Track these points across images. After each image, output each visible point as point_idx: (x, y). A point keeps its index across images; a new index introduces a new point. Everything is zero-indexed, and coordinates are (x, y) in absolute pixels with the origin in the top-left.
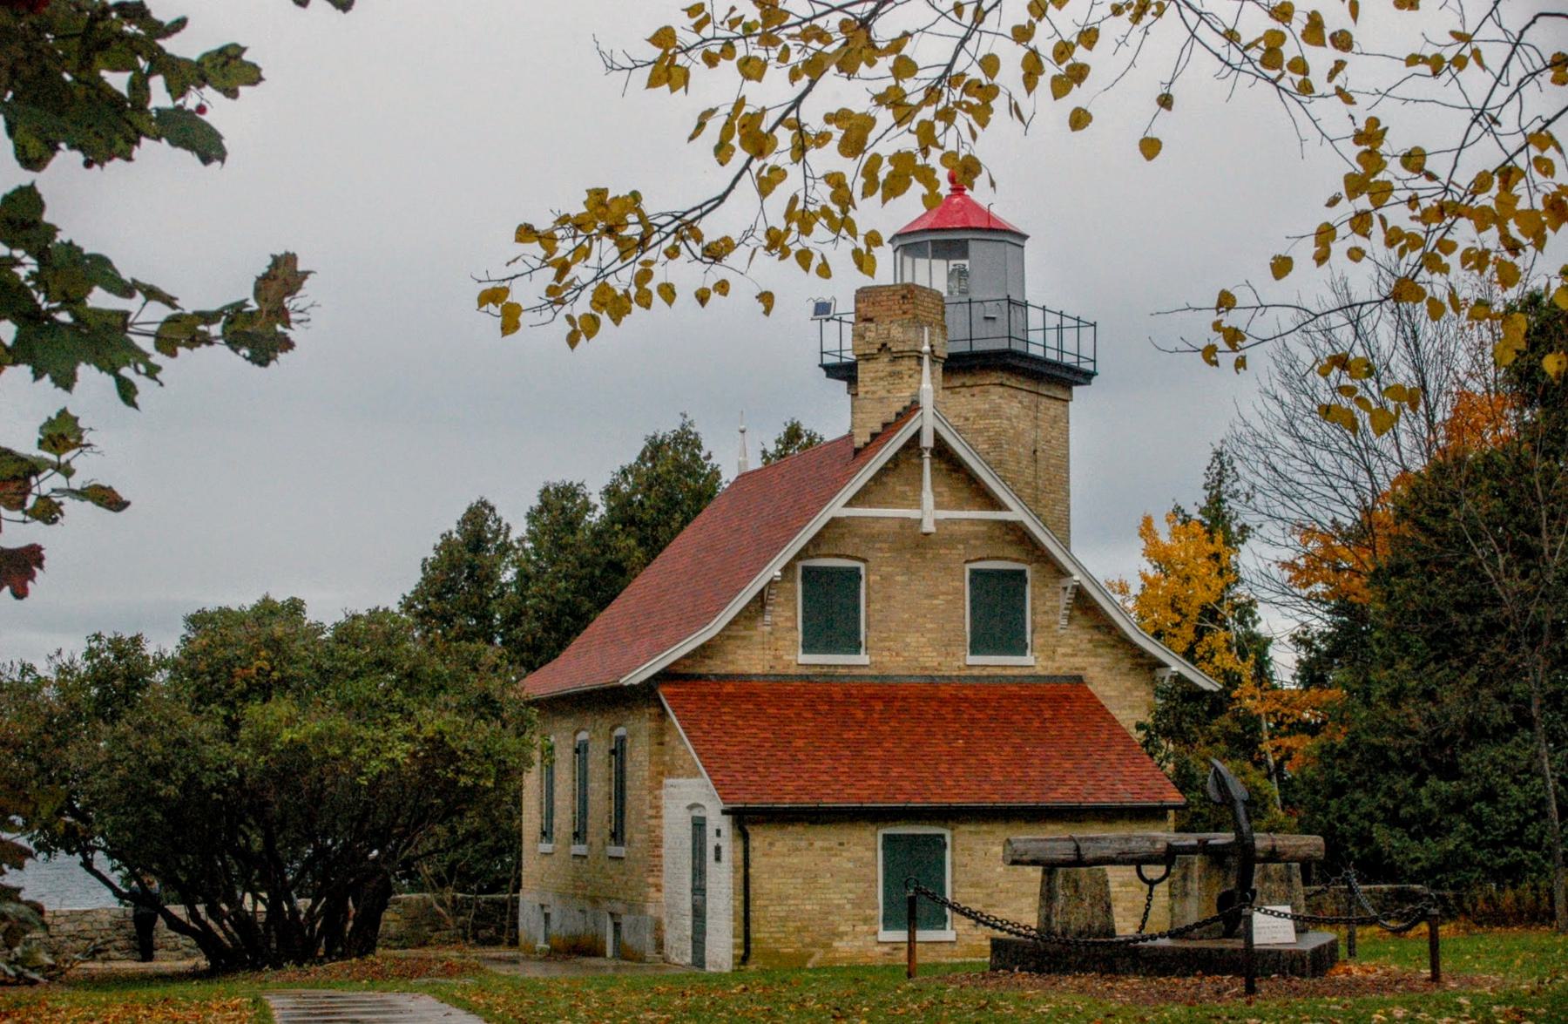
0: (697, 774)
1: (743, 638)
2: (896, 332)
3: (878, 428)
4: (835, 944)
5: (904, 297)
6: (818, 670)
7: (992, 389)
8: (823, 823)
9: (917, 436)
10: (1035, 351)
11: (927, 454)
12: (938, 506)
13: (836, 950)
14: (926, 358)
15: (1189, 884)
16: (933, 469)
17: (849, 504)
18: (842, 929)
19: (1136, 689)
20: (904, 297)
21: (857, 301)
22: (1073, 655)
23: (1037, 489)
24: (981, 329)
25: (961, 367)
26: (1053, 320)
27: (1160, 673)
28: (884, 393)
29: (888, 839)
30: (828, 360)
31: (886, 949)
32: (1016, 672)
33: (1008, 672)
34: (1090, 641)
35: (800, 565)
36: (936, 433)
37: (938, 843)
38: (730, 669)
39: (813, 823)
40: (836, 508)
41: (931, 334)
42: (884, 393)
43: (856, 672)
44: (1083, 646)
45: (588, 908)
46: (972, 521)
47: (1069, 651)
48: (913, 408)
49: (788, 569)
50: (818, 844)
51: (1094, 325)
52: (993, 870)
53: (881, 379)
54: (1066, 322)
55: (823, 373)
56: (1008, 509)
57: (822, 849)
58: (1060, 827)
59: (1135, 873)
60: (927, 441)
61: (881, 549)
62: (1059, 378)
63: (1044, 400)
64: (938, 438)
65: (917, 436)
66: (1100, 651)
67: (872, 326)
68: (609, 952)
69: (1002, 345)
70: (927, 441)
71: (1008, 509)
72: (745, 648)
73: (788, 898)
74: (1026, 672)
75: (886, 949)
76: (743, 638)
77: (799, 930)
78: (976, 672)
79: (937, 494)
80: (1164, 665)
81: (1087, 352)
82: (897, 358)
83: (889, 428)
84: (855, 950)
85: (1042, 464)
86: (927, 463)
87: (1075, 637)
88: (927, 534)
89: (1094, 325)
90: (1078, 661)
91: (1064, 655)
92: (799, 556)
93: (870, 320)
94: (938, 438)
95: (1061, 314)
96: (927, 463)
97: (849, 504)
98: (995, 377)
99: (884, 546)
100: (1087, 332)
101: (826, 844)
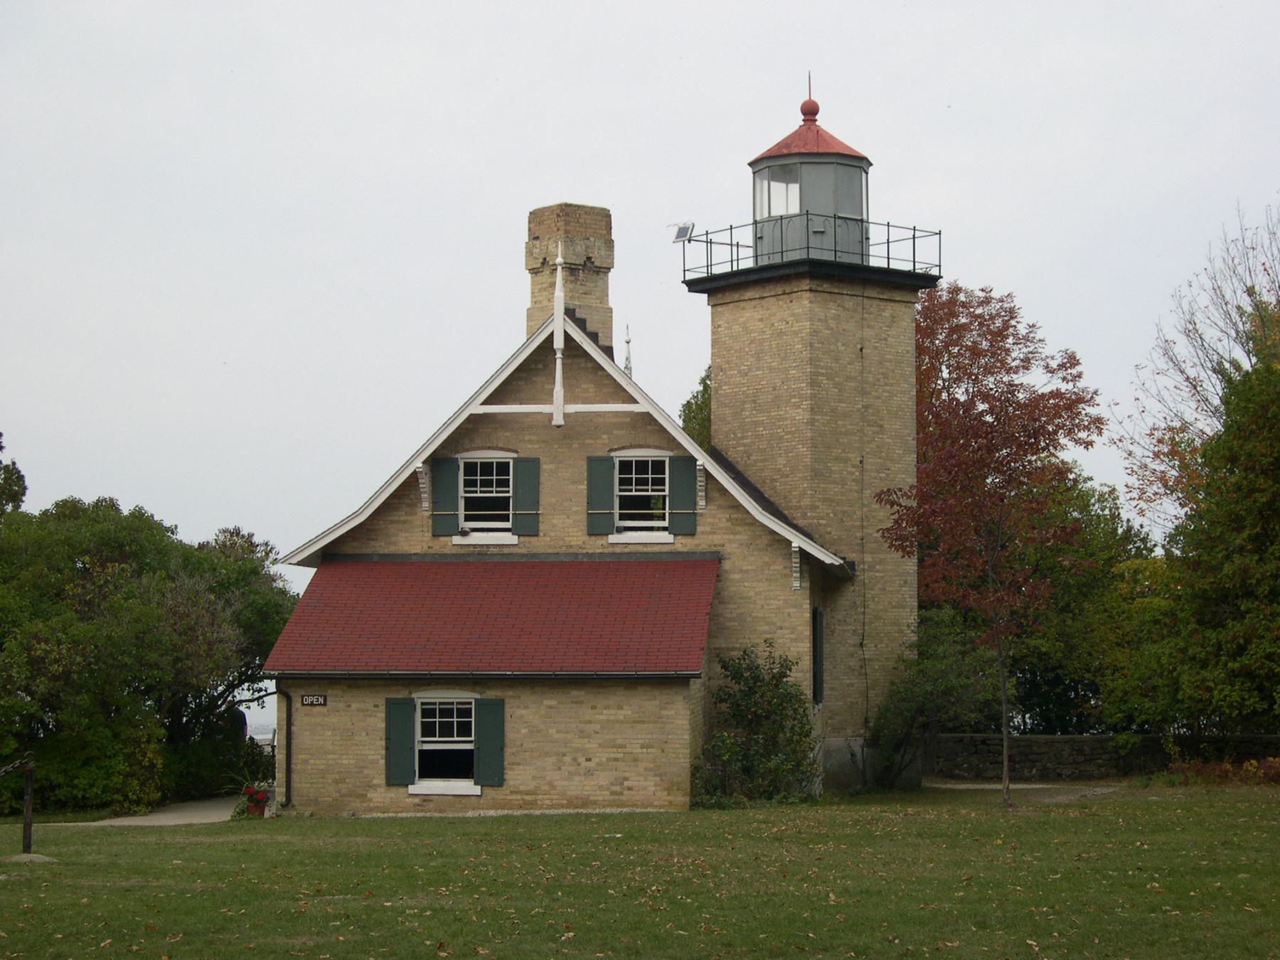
1: (405, 522)
8: (358, 687)
11: (559, 355)
12: (568, 400)
13: (371, 800)
17: (485, 403)
18: (375, 782)
19: (774, 563)
29: (387, 699)
30: (690, 276)
31: (417, 800)
32: (656, 549)
34: (728, 520)
35: (465, 457)
37: (500, 704)
38: (392, 549)
39: (350, 687)
43: (506, 551)
44: (721, 525)
45: (588, 764)
46: (616, 414)
47: (708, 529)
50: (354, 706)
55: (685, 288)
57: (358, 710)
58: (583, 693)
60: (559, 343)
61: (530, 441)
64: (568, 338)
66: (739, 528)
70: (559, 343)
71: (635, 402)
74: (665, 549)
75: (417, 800)
76: (405, 522)
77: (336, 782)
78: (618, 550)
86: (559, 362)
87: (714, 516)
88: (559, 427)
90: (717, 539)
91: (702, 533)
96: (559, 362)
98: (806, 284)
99: (533, 438)
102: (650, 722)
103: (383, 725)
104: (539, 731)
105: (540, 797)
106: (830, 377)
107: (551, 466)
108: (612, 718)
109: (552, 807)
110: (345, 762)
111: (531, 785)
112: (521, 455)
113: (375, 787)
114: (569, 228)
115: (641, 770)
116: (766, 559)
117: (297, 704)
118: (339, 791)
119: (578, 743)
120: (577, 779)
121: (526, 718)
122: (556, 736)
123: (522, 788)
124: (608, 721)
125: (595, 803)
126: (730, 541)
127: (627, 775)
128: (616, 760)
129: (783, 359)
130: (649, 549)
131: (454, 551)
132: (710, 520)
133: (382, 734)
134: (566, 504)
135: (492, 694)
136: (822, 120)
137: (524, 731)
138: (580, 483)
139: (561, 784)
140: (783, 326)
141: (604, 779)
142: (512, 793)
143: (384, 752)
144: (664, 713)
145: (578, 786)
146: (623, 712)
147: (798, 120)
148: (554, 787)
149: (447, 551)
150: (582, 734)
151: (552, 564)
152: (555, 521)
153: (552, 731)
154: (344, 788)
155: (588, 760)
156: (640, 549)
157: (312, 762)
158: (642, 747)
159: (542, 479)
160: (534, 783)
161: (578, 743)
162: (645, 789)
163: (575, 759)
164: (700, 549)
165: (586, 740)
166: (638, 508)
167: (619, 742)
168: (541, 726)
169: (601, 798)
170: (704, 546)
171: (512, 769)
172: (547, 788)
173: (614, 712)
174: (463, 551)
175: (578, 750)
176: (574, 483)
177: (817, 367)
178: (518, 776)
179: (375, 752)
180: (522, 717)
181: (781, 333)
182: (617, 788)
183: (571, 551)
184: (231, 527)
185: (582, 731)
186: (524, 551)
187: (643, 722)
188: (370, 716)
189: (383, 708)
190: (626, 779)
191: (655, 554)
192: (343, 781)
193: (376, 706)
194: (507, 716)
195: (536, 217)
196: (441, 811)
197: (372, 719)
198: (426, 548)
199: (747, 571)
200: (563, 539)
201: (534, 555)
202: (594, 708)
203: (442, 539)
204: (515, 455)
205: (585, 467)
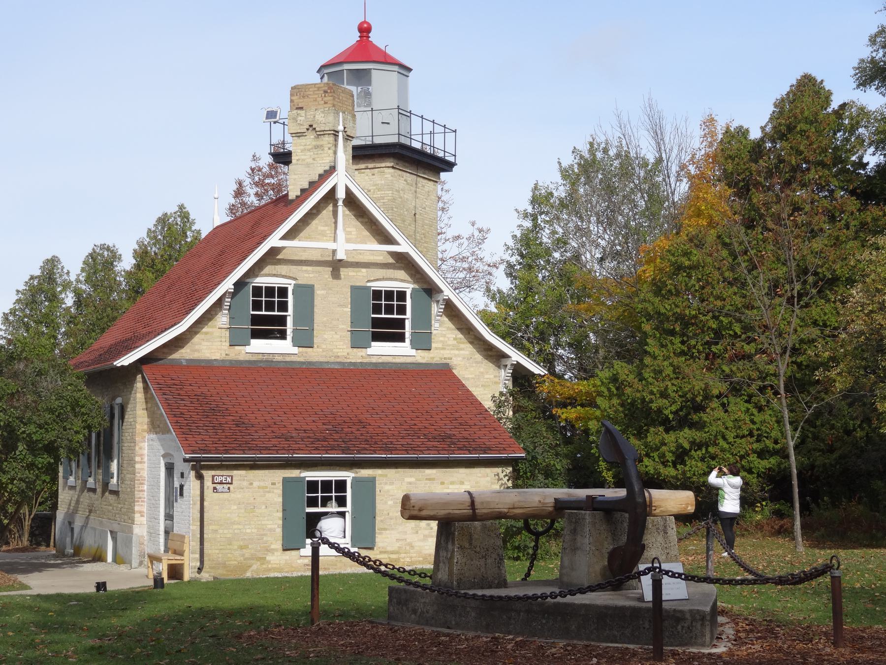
0: (169, 431)
2: (320, 117)
3: (306, 185)
4: (268, 558)
5: (325, 92)
6: (261, 357)
7: (387, 170)
9: (333, 191)
10: (416, 145)
11: (340, 203)
12: (348, 241)
13: (269, 562)
14: (341, 134)
15: (579, 538)
16: (344, 215)
18: (273, 547)
20: (325, 92)
21: (292, 95)
22: (444, 349)
24: (379, 129)
25: (364, 154)
26: (428, 127)
27: (505, 361)
28: (310, 161)
38: (196, 356)
40: (274, 240)
41: (344, 120)
42: (310, 161)
43: (288, 359)
44: (450, 343)
47: (440, 345)
48: (333, 169)
49: (240, 285)
50: (256, 484)
51: (455, 131)
52: (386, 503)
53: (309, 150)
54: (438, 129)
56: (398, 244)
57: (259, 487)
60: (341, 194)
62: (431, 165)
63: (421, 180)
64: (348, 192)
65: (333, 191)
66: (462, 346)
67: (302, 112)
68: (110, 558)
69: (394, 139)
70: (341, 194)
71: (398, 244)
72: (208, 340)
73: (233, 523)
79: (348, 233)
80: (508, 357)
81: (450, 149)
82: (320, 134)
83: (314, 186)
84: (283, 562)
85: (419, 222)
88: (340, 261)
89: (455, 131)
90: (446, 353)
91: (436, 348)
92: (253, 272)
93: (301, 108)
94: (348, 192)
95: (433, 122)
97: (284, 238)
100: (450, 136)
101: (262, 484)
103: (281, 499)
107: (323, 292)
110: (248, 531)
111: (395, 546)
112: (300, 282)
113: (272, 551)
116: (482, 370)
117: (208, 483)
118: (243, 555)
123: (389, 549)
126: (456, 356)
130: (398, 360)
131: (247, 359)
132: (442, 339)
133: (280, 508)
134: (334, 322)
135: (365, 473)
136: (374, 37)
137: (390, 503)
138: (344, 306)
142: (381, 552)
143: (281, 522)
147: (355, 36)
148: (412, 547)
149: (241, 358)
151: (302, 370)
152: (326, 336)
154: (247, 553)
156: (390, 360)
157: (221, 531)
159: (316, 302)
160: (398, 545)
164: (434, 361)
166: (388, 330)
171: (380, 534)
173: (457, 486)
174: (254, 358)
176: (340, 306)
179: (274, 522)
180: (388, 491)
183: (338, 360)
186: (301, 359)
188: (269, 492)
189: (280, 486)
191: (401, 364)
192: (246, 547)
193: (273, 484)
194: (378, 492)
195: (292, 88)
200: (331, 350)
201: (310, 363)
202: (442, 483)
203: (237, 347)
204: (293, 282)
205: (349, 294)
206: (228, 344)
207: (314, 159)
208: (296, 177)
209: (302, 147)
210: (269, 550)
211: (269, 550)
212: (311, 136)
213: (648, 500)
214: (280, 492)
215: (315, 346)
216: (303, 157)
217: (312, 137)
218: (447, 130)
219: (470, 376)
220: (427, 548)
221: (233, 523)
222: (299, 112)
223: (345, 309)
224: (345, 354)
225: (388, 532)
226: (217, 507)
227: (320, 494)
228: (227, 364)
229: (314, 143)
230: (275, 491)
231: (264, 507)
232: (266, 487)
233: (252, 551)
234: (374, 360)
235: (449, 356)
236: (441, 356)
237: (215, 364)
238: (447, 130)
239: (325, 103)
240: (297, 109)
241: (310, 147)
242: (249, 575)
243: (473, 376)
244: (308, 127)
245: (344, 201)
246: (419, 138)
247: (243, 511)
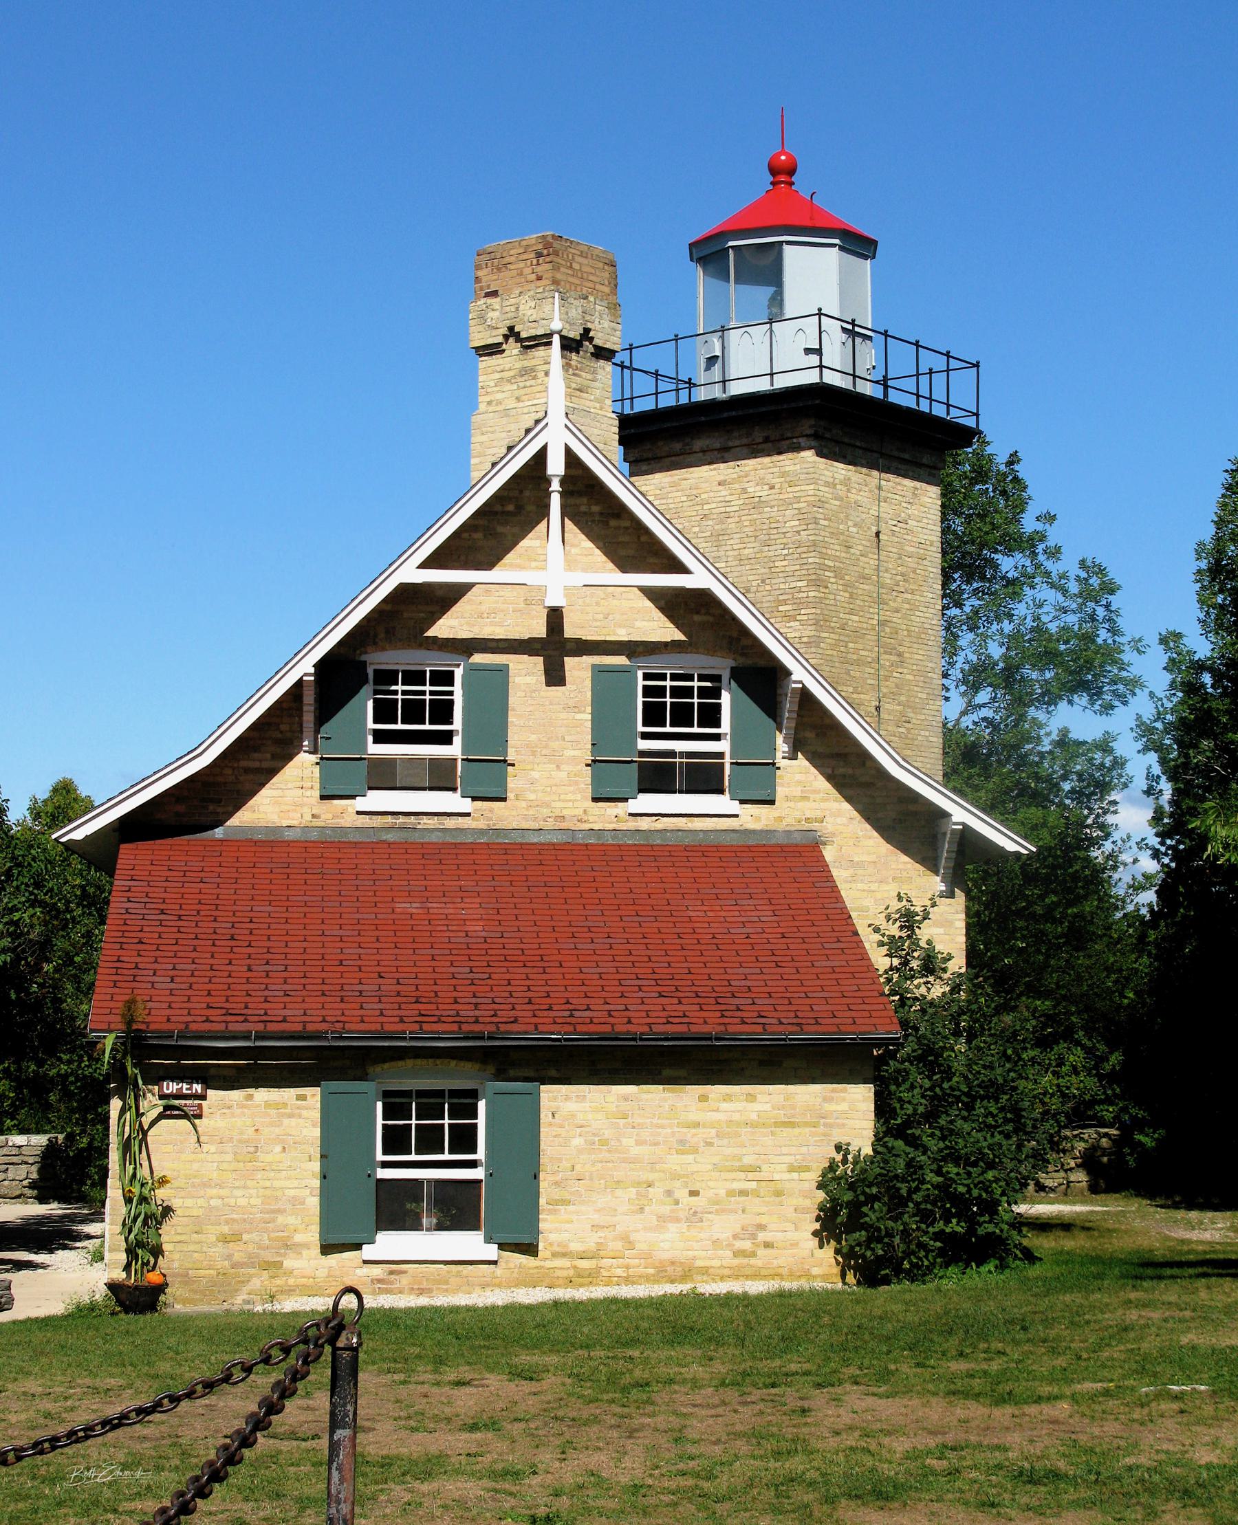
4: (288, 1264)
5: (539, 255)
11: (555, 485)
17: (424, 565)
18: (298, 1238)
23: (879, 585)
28: (511, 403)
33: (698, 824)
36: (569, 452)
42: (511, 403)
47: (797, 791)
51: (977, 365)
53: (509, 381)
59: (365, 1301)
60: (556, 466)
64: (571, 459)
70: (556, 466)
71: (686, 571)
73: (206, 1185)
75: (377, 1271)
77: (225, 1239)
89: (977, 365)
90: (810, 809)
91: (788, 798)
93: (494, 294)
94: (571, 459)
95: (917, 344)
102: (806, 1124)
103: (317, 1132)
104: (604, 1142)
105: (606, 1262)
106: (839, 574)
108: (736, 1117)
109: (629, 1280)
110: (242, 1202)
111: (590, 1243)
114: (559, 276)
115: (790, 1213)
118: (229, 1257)
119: (675, 1162)
120: (673, 1227)
121: (574, 1114)
122: (636, 1151)
123: (575, 1247)
124: (730, 1122)
125: (705, 1271)
127: (764, 1220)
128: (743, 1193)
129: (766, 544)
132: (798, 777)
134: (555, 745)
136: (803, 184)
137: (577, 1142)
138: (577, 709)
139: (643, 1240)
140: (764, 492)
141: (724, 1227)
143: (317, 1183)
144: (829, 1107)
145: (671, 1243)
146: (756, 1106)
148: (630, 1244)
150: (684, 1148)
152: (535, 775)
153: (628, 1142)
155: (694, 1193)
158: (792, 1169)
159: (512, 701)
161: (675, 1162)
162: (794, 1245)
163: (669, 1193)
164: (781, 827)
165: (690, 1158)
167: (747, 1160)
168: (608, 1133)
169: (716, 1263)
170: (789, 820)
172: (619, 1245)
175: (675, 1176)
177: (823, 556)
178: (557, 1227)
181: (758, 504)
182: (746, 1245)
183: (564, 825)
184: (1113, 574)
185: (682, 1142)
187: (792, 1125)
188: (291, 1116)
190: (762, 1227)
192: (236, 1238)
196: (422, 1292)
197: (293, 1121)
198: (308, 817)
199: (861, 865)
200: (548, 806)
205: (588, 683)
206: (317, 794)
207: (518, 399)
208: (484, 438)
209: (497, 376)
210: (288, 1246)
211: (288, 1246)
212: (512, 348)
213: (78, 1244)
214: (317, 1115)
215: (510, 795)
216: (499, 396)
217: (516, 352)
218: (954, 364)
219: (865, 858)
220: (666, 1245)
221: (206, 1185)
222: (490, 301)
223: (579, 716)
224: (579, 812)
225: (571, 1208)
226: (169, 1148)
227: (414, 1122)
228: (314, 836)
229: (518, 365)
230: (305, 1113)
231: (278, 1149)
232: (285, 1105)
233: (250, 1248)
234: (645, 824)
235: (819, 814)
236: (798, 814)
237: (289, 835)
238: (954, 364)
239: (539, 278)
240: (488, 295)
241: (511, 373)
242: (238, 1302)
243: (873, 858)
244: (505, 331)
245: (563, 482)
246: (910, 385)
247: (229, 1157)
